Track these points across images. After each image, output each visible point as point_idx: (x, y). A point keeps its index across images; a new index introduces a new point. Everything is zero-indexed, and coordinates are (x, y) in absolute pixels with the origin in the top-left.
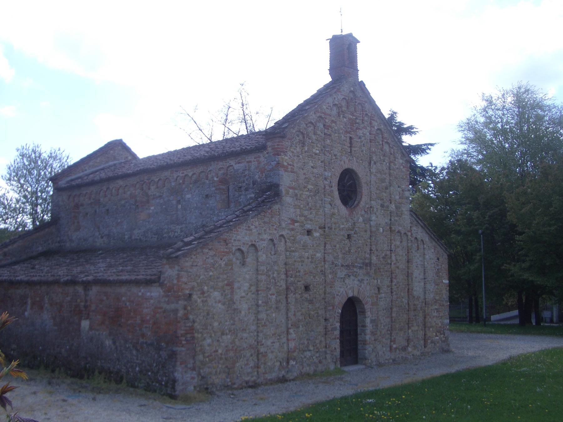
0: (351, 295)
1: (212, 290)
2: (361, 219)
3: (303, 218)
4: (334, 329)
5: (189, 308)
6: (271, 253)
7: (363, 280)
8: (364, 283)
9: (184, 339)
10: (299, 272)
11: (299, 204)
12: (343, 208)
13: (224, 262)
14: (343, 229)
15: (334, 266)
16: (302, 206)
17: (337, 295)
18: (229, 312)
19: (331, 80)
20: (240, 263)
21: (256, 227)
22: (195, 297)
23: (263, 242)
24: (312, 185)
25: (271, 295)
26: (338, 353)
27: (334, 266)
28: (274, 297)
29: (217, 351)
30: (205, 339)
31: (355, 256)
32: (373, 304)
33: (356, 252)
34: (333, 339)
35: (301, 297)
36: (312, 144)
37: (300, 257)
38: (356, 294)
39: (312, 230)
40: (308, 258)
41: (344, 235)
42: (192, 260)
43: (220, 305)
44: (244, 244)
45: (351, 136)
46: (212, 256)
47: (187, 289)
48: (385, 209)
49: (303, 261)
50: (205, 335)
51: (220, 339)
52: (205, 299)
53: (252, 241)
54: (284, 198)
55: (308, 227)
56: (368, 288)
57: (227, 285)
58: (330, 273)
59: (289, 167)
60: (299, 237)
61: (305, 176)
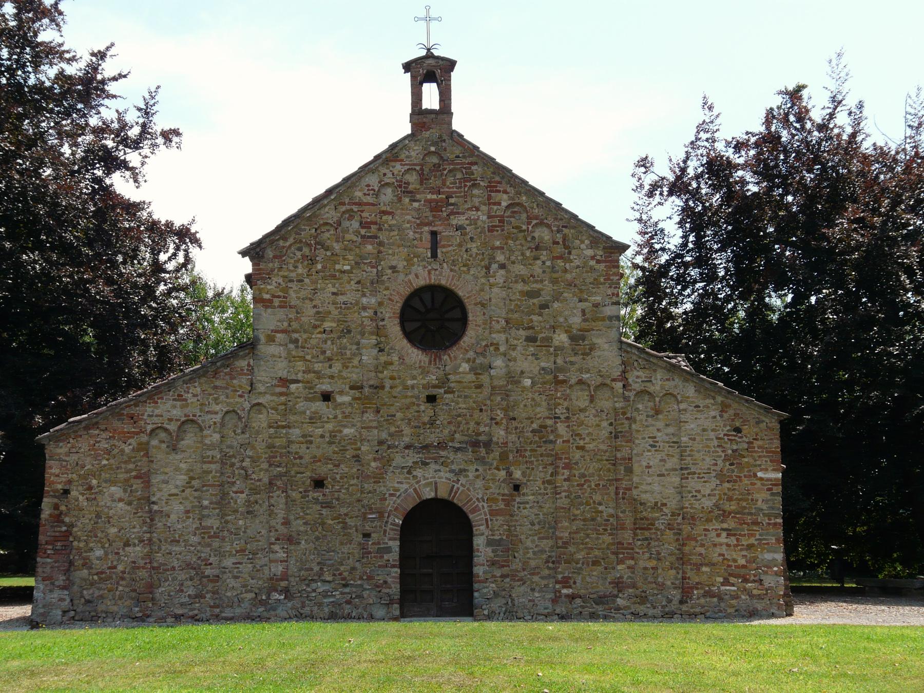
1: (104, 485)
2: (465, 367)
3: (311, 376)
4: (388, 550)
5: (63, 508)
6: (234, 431)
8: (467, 476)
9: (50, 547)
10: (301, 458)
11: (301, 354)
13: (131, 447)
18: (139, 515)
20: (168, 447)
22: (74, 493)
24: (333, 320)
25: (236, 492)
26: (395, 589)
29: (115, 567)
30: (92, 549)
36: (335, 258)
37: (304, 436)
39: (333, 392)
42: (69, 445)
44: (170, 420)
45: (435, 229)
46: (106, 439)
47: (60, 483)
48: (538, 343)
50: (91, 545)
51: (121, 551)
52: (93, 496)
53: (186, 416)
55: (326, 387)
57: (136, 477)
58: (375, 460)
59: (275, 300)
60: (301, 405)
61: (315, 310)
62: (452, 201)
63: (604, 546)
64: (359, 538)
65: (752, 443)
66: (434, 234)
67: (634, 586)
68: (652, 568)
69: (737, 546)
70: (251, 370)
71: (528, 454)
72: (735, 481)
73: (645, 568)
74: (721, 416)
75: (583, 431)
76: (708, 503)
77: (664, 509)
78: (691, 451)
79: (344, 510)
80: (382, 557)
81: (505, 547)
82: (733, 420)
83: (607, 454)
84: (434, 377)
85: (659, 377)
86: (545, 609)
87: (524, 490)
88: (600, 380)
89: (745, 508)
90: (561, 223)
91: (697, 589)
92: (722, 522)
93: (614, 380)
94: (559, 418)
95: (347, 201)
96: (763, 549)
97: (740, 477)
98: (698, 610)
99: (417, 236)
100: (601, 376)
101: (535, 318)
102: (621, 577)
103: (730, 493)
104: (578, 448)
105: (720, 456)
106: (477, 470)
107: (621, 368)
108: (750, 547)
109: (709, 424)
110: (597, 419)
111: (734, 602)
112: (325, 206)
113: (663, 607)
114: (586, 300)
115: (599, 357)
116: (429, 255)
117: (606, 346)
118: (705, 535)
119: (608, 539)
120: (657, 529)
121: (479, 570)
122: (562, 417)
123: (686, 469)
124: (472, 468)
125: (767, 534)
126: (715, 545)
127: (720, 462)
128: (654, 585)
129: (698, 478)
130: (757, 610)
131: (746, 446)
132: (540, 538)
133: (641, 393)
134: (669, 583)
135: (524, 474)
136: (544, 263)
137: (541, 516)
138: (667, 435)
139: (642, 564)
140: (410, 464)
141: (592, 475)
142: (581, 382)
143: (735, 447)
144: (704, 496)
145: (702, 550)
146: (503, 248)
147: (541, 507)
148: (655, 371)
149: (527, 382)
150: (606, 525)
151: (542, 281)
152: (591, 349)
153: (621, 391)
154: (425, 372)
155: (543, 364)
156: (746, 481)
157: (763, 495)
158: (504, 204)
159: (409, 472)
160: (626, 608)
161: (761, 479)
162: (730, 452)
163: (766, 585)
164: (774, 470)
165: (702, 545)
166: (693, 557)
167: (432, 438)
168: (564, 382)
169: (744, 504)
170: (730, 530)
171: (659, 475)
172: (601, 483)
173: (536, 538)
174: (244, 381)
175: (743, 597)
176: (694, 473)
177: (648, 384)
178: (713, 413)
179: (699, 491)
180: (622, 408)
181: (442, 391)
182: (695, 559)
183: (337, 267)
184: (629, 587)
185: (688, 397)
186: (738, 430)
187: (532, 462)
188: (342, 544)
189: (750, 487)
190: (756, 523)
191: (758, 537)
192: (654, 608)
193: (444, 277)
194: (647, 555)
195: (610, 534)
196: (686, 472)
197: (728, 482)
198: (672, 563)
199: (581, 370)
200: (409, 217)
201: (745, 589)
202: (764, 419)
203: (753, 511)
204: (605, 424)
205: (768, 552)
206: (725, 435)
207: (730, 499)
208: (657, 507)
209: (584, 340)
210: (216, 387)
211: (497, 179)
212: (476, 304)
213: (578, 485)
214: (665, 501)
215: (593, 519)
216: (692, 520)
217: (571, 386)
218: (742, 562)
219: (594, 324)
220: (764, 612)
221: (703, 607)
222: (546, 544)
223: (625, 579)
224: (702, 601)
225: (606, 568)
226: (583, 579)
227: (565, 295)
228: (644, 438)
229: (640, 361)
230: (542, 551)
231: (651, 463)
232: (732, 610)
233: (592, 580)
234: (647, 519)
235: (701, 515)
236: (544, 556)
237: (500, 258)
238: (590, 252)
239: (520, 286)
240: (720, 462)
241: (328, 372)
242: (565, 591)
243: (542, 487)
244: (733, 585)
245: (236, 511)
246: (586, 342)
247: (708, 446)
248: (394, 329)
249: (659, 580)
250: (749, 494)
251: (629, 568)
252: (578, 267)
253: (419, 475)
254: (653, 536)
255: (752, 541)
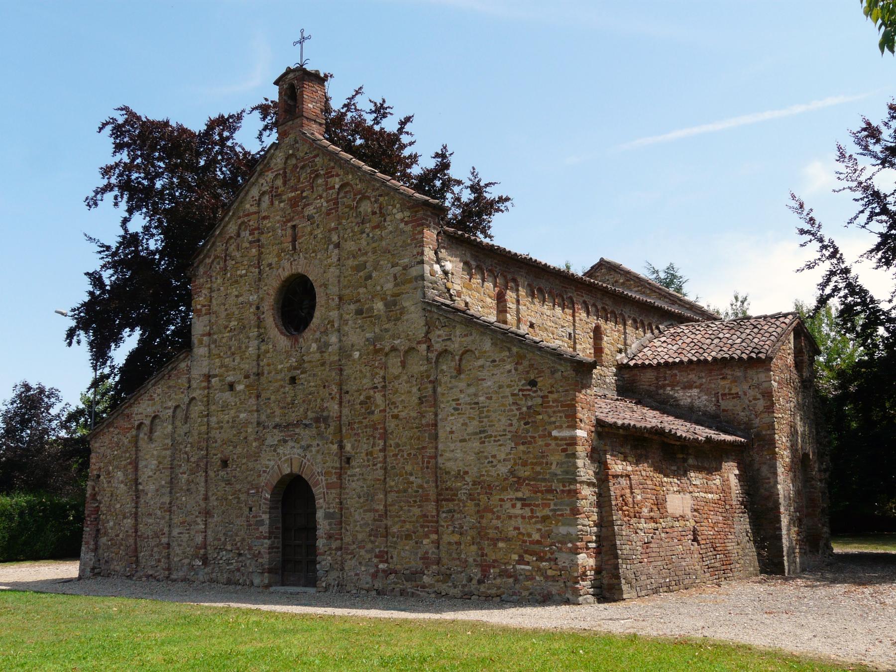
0: (287, 471)
2: (314, 346)
4: (261, 523)
5: (97, 489)
7: (309, 446)
8: (311, 451)
12: (283, 342)
14: (281, 371)
15: (261, 428)
16: (222, 354)
17: (264, 472)
19: (580, 274)
21: (159, 395)
22: (102, 477)
23: (167, 411)
27: (261, 428)
28: (185, 476)
31: (301, 410)
32: (329, 486)
33: (304, 401)
34: (258, 538)
35: (216, 476)
37: (218, 423)
38: (296, 470)
40: (228, 422)
41: (283, 380)
43: (122, 485)
44: (146, 416)
45: (294, 223)
48: (364, 315)
49: (222, 428)
54: (195, 350)
55: (230, 379)
56: (319, 457)
58: (255, 440)
62: (305, 194)
63: (414, 519)
64: (246, 511)
65: (547, 397)
66: (294, 227)
67: (438, 562)
68: (456, 543)
69: (531, 517)
70: (189, 369)
71: (356, 426)
72: (530, 443)
73: (449, 543)
74: (516, 369)
75: (397, 399)
76: (503, 469)
77: (466, 478)
78: (488, 411)
79: (238, 487)
80: (258, 529)
81: (340, 518)
82: (528, 372)
83: (417, 421)
84: (294, 360)
85: (458, 333)
86: (367, 583)
87: (353, 463)
88: (408, 344)
89: (539, 473)
90: (377, 193)
91: (494, 567)
92: (517, 490)
93: (419, 343)
94: (376, 387)
95: (241, 214)
96: (557, 522)
97: (534, 437)
98: (493, 591)
99: (284, 232)
100: (409, 340)
101: (362, 290)
102: (426, 553)
103: (525, 457)
104: (393, 417)
105: (515, 415)
106: (318, 445)
107: (424, 329)
108: (545, 519)
109: (504, 379)
110: (408, 385)
111: (528, 583)
112: (228, 222)
113: (464, 586)
114: (397, 265)
115: (407, 321)
116: (291, 248)
117: (413, 308)
118: (501, 506)
119: (416, 511)
120: (459, 500)
121: (321, 543)
122: (379, 386)
123: (484, 431)
124: (315, 443)
125: (561, 504)
126: (510, 517)
127: (515, 422)
128: (458, 563)
129: (495, 441)
130: (552, 595)
131: (539, 401)
132: (365, 511)
133: (445, 352)
134: (471, 560)
135: (353, 447)
136: (368, 235)
137: (365, 489)
138: (469, 396)
139: (446, 538)
140: (276, 443)
141: (405, 444)
142: (394, 349)
143: (530, 403)
144: (499, 461)
145: (498, 523)
146: (337, 228)
147: (365, 479)
148: (454, 327)
149: (356, 355)
150: (416, 496)
151: (366, 253)
152: (401, 314)
153: (425, 353)
154: (288, 355)
155: (368, 335)
156: (540, 442)
157: (557, 457)
158: (337, 186)
159: (275, 451)
160: (432, 586)
161: (556, 438)
162: (524, 409)
163: (561, 564)
164: (568, 427)
165: (498, 518)
166: (490, 531)
167: (293, 417)
168: (382, 349)
169: (538, 469)
170: (525, 500)
171: (461, 441)
172: (413, 452)
173: (361, 511)
174: (183, 380)
175: (538, 578)
176: (491, 436)
177: (448, 343)
178: (508, 367)
179: (494, 456)
180: (426, 371)
181: (299, 372)
182: (492, 533)
183: (239, 273)
184: (433, 564)
185: (485, 352)
186: (533, 383)
187: (358, 434)
188: (237, 517)
189: (544, 448)
190: (550, 491)
191: (552, 507)
192: (455, 588)
193: (301, 266)
194: (451, 528)
195: (420, 506)
196: (483, 435)
197: (523, 444)
198: (473, 538)
199: (393, 337)
200: (278, 217)
201: (539, 569)
202: (559, 367)
203: (547, 477)
204: (415, 390)
205: (563, 525)
206: (520, 390)
207: (525, 464)
208: (460, 475)
209: (395, 305)
210: (169, 387)
211: (332, 164)
212: (321, 286)
213: (393, 455)
214: (466, 469)
215: (405, 491)
216: (489, 489)
217: (387, 355)
218: (536, 536)
219: (403, 287)
220: (557, 597)
221: (499, 588)
222: (369, 516)
223: (430, 555)
224: (498, 581)
225: (417, 543)
226: (399, 553)
227: (381, 263)
228: (448, 402)
229: (441, 318)
230: (367, 524)
231: (454, 428)
232: (525, 593)
233: (405, 556)
234: (452, 490)
235: (496, 484)
236: (368, 530)
237: (335, 238)
238: (399, 216)
239: (351, 262)
240: (515, 422)
241: (232, 365)
242: (381, 566)
243: (366, 458)
244: (528, 563)
245: (182, 489)
246: (397, 307)
247: (503, 405)
248: (270, 320)
249: (463, 556)
250: (543, 457)
251: (432, 542)
252: (391, 232)
253: (281, 452)
254: (456, 508)
255: (547, 512)
